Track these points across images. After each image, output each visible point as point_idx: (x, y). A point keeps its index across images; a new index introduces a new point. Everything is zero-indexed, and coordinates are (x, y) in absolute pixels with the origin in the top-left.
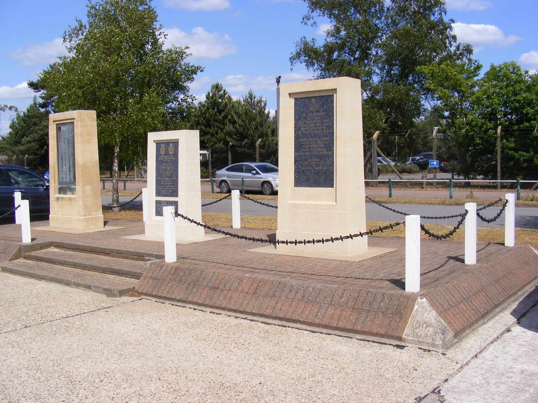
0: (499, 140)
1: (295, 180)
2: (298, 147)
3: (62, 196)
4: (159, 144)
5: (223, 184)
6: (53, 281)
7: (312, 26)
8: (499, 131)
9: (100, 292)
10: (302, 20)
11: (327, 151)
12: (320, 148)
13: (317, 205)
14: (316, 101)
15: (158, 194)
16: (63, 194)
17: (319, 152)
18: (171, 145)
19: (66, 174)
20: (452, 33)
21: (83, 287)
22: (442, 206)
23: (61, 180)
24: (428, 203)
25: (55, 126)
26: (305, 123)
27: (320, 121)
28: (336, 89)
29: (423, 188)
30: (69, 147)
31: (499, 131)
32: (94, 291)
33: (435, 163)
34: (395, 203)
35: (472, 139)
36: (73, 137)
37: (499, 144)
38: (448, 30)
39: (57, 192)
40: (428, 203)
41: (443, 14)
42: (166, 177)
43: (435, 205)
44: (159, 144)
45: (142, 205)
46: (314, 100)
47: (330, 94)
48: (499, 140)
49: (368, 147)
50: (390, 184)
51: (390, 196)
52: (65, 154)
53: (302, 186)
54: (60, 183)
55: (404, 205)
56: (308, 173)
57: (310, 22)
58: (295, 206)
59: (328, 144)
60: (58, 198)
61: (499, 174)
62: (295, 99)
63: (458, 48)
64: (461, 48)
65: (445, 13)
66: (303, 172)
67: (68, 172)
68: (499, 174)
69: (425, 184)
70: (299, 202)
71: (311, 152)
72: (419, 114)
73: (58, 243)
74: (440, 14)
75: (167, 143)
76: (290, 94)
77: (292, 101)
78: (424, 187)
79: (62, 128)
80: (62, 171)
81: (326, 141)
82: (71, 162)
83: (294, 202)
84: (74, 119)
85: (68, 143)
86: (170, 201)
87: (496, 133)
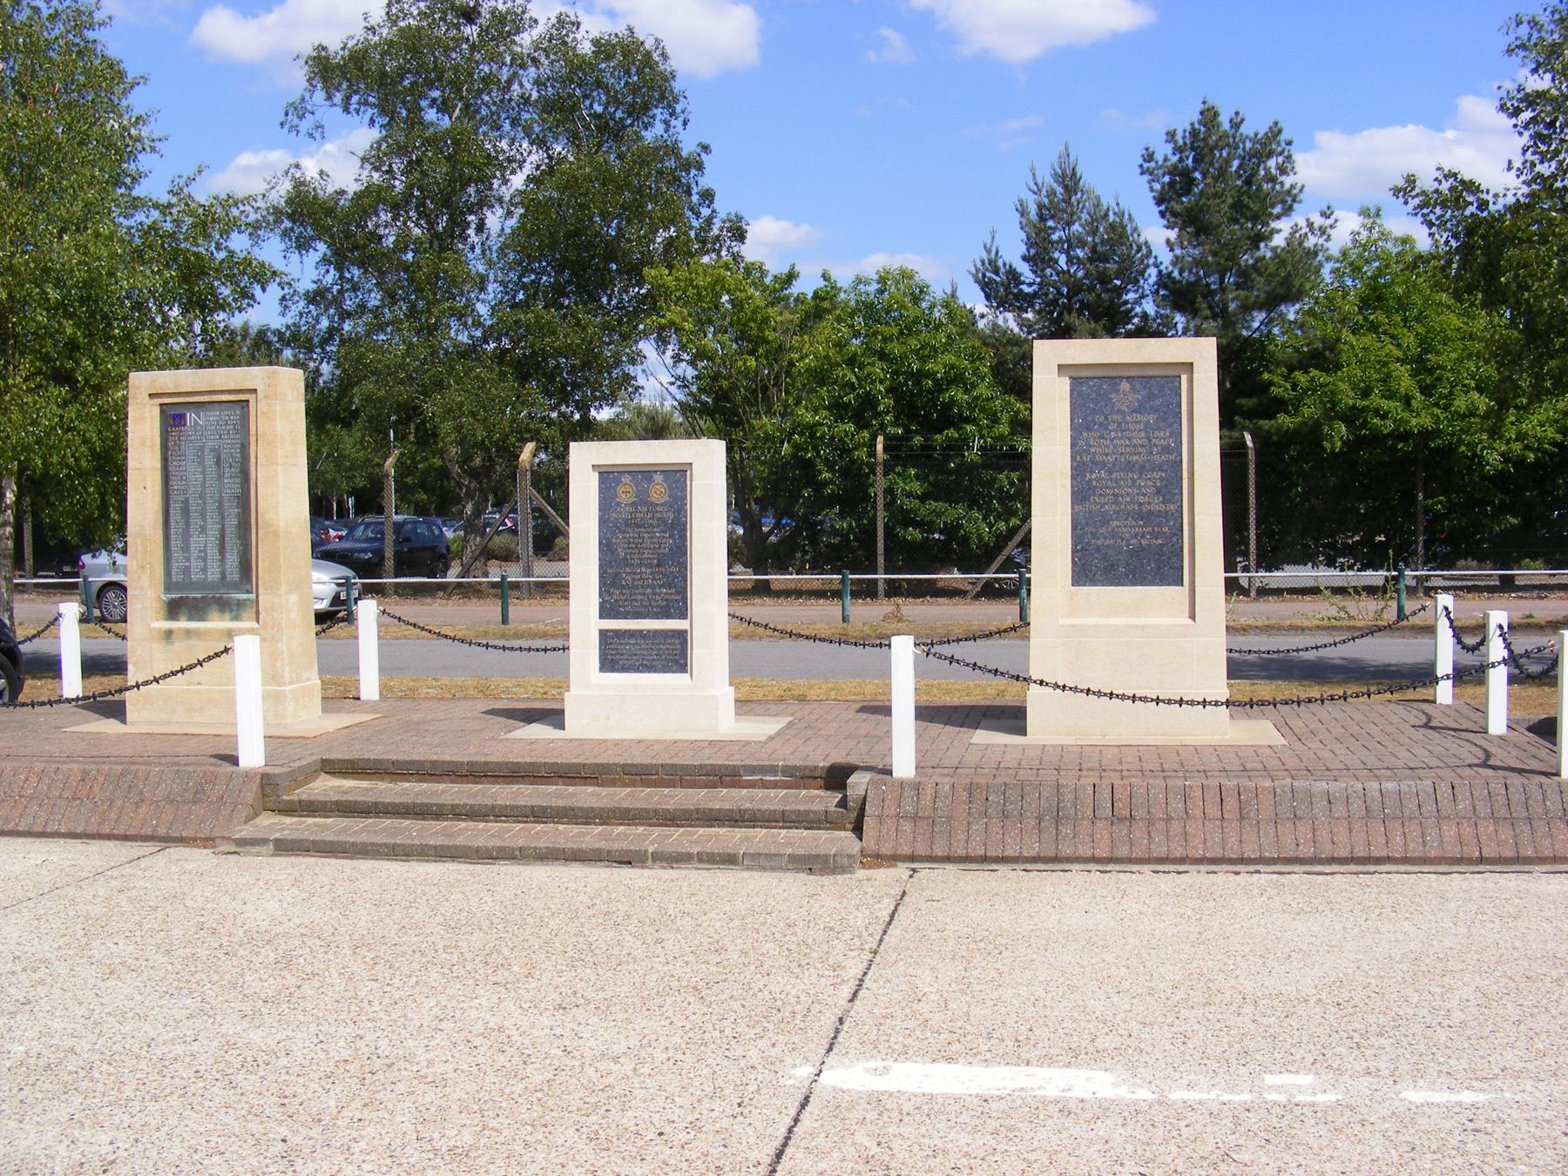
0: (879, 470)
2: (1081, 493)
3: (182, 624)
4: (678, 476)
5: (111, 595)
6: (557, 859)
7: (311, 135)
8: (880, 447)
9: (781, 869)
10: (282, 118)
13: (1143, 627)
14: (1133, 388)
15: (606, 611)
16: (190, 619)
18: (658, 478)
19: (204, 559)
21: (700, 861)
23: (177, 577)
25: (157, 411)
26: (1102, 437)
27: (1143, 434)
30: (220, 477)
31: (880, 447)
32: (748, 868)
35: (808, 466)
36: (244, 448)
37: (880, 483)
39: (162, 613)
42: (641, 565)
44: (609, 477)
45: (59, 662)
46: (1125, 386)
47: (1171, 372)
48: (879, 470)
49: (468, 487)
50: (503, 590)
51: (505, 620)
52: (202, 496)
53: (1093, 582)
54: (169, 586)
56: (1110, 552)
57: (306, 124)
60: (169, 634)
61: (881, 560)
67: (213, 553)
68: (881, 560)
69: (881, 587)
70: (1092, 621)
71: (1116, 502)
72: (610, 399)
73: (351, 762)
75: (644, 474)
76: (1060, 366)
77: (1065, 384)
79: (191, 417)
80: (186, 548)
81: (1161, 479)
82: (232, 522)
83: (1078, 621)
84: (255, 391)
85: (218, 463)
86: (673, 631)
87: (872, 454)
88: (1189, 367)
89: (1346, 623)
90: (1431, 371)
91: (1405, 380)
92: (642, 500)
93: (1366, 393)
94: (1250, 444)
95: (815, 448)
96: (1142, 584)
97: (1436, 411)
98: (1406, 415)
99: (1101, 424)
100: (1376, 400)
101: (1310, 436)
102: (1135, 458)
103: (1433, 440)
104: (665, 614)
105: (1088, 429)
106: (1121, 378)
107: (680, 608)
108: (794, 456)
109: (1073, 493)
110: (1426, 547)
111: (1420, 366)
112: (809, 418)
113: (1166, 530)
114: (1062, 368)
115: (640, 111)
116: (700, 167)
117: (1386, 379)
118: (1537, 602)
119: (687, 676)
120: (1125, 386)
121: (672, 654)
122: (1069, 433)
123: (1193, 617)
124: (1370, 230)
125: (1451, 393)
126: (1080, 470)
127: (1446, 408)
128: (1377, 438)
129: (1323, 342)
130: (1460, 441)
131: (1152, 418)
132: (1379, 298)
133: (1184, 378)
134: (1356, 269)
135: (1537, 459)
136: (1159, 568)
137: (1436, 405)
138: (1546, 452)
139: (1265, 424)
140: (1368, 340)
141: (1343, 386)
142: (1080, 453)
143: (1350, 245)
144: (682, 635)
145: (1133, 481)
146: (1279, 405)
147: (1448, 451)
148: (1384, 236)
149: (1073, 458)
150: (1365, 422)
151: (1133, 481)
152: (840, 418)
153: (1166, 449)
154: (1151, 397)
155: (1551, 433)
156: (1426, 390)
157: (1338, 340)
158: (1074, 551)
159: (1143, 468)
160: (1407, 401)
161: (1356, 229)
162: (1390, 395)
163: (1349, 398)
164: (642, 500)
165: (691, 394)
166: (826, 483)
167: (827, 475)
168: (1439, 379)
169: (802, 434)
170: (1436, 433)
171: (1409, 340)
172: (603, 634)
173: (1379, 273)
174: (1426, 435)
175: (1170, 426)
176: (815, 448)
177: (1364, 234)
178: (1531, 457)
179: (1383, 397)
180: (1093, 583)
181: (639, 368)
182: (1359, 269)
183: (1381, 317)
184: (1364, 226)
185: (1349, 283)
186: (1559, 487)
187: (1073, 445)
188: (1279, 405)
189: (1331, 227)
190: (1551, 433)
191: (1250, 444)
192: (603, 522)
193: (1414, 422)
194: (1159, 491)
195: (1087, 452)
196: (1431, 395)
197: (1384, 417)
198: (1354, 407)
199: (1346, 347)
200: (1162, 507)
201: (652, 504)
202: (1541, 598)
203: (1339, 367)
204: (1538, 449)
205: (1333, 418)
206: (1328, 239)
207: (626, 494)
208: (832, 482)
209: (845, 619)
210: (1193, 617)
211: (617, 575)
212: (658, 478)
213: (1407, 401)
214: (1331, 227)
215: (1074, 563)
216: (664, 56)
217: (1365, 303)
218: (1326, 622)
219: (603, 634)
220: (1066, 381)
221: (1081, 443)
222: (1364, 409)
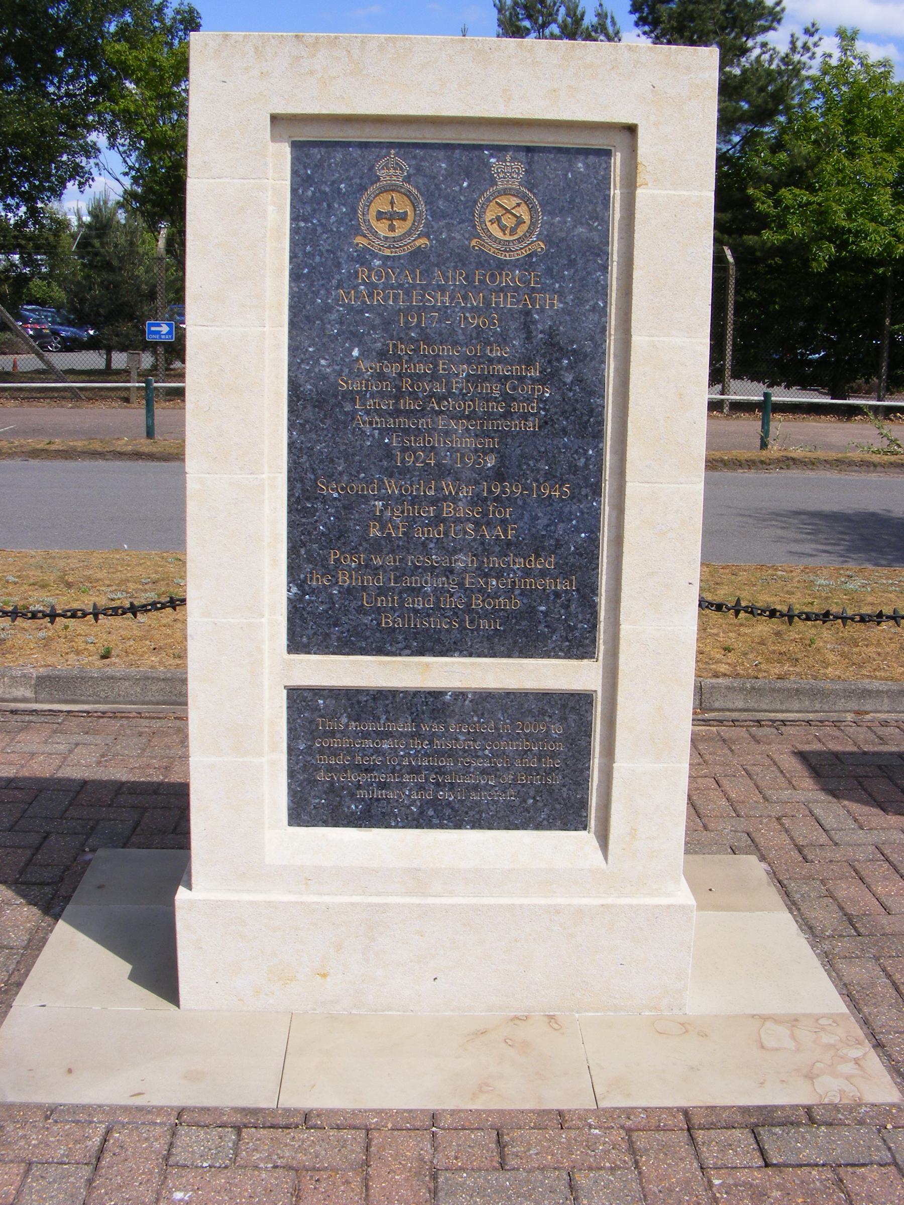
4: (577, 168)
15: (309, 628)
18: (508, 172)
29: (127, 400)
33: (165, 329)
75: (450, 159)
92: (449, 253)
94: (731, 259)
101: (795, 253)
104: (522, 635)
107: (569, 616)
110: (890, 368)
119: (586, 839)
121: (542, 773)
139: (750, 239)
146: (763, 222)
164: (449, 253)
172: (301, 700)
181: (92, 161)
188: (763, 222)
191: (731, 259)
192: (302, 316)
201: (485, 261)
205: (821, 239)
207: (389, 221)
211: (349, 505)
212: (508, 172)
219: (301, 700)
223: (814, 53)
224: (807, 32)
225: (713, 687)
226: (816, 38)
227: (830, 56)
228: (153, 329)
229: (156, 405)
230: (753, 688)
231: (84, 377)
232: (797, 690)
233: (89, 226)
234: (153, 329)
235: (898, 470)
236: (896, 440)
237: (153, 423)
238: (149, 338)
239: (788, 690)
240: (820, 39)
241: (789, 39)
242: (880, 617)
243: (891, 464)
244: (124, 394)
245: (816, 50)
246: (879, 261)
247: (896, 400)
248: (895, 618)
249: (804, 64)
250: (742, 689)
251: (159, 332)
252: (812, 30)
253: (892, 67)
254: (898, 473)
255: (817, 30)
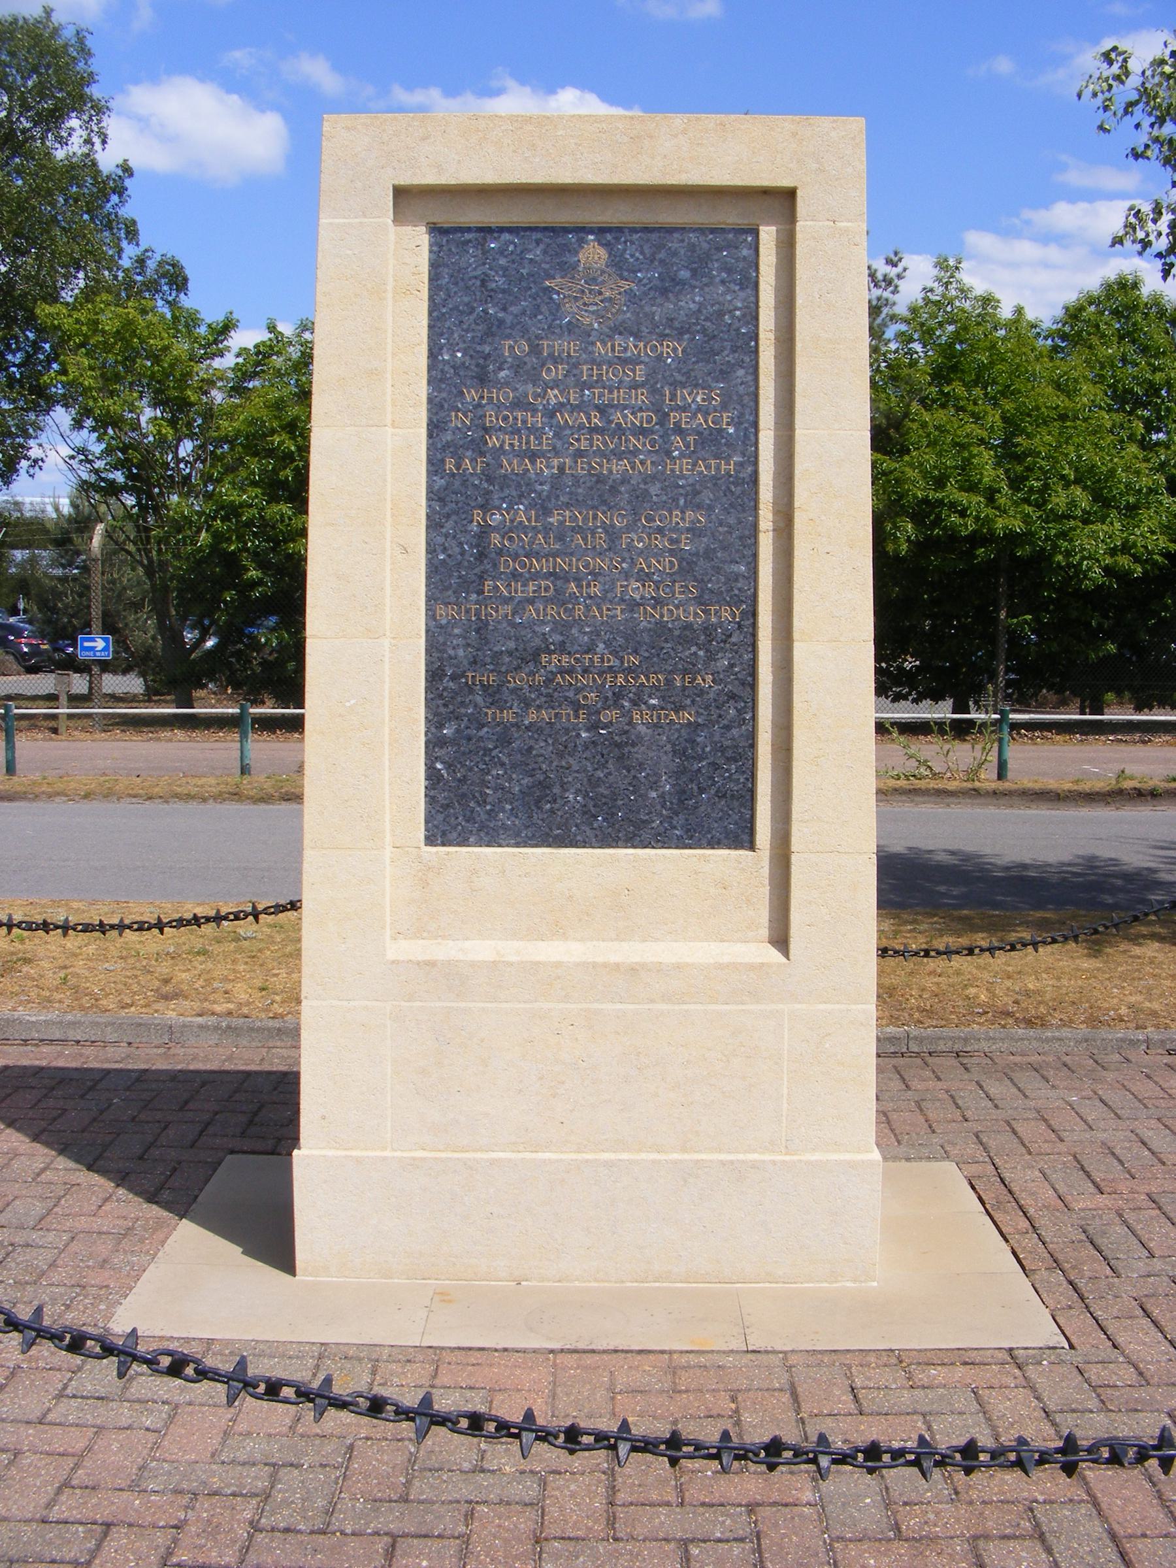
1: (431, 799)
2: (460, 563)
11: (700, 601)
12: (644, 577)
13: (634, 970)
14: (617, 264)
17: (633, 605)
20: (126, 212)
22: (232, 807)
24: (177, 796)
26: (519, 404)
27: (641, 397)
28: (790, 195)
29: (55, 731)
33: (100, 644)
34: (50, 796)
35: (232, 563)
38: (115, 199)
40: (177, 796)
41: (97, 140)
43: (204, 800)
46: (593, 254)
47: (729, 216)
55: (86, 806)
56: (542, 747)
58: (451, 978)
59: (708, 554)
62: (436, 230)
63: (141, 262)
64: (151, 265)
65: (104, 142)
66: (504, 740)
70: (481, 950)
71: (560, 599)
74: (88, 141)
76: (401, 194)
77: (412, 249)
78: (62, 729)
81: (695, 532)
83: (444, 950)
88: (783, 201)
89: (933, 784)
90: (1018, 458)
91: (988, 470)
93: (940, 483)
95: (241, 538)
96: (632, 841)
97: (1028, 509)
98: (990, 511)
99: (518, 367)
100: (952, 492)
102: (618, 467)
103: (1022, 546)
105: (482, 379)
106: (582, 230)
108: (214, 548)
109: (434, 570)
111: (1008, 454)
112: (234, 497)
113: (705, 681)
114: (407, 199)
115: (53, 119)
116: (121, 191)
117: (965, 466)
118: (1140, 746)
120: (593, 254)
122: (421, 389)
123: (781, 941)
124: (947, 284)
125: (1046, 486)
126: (453, 501)
127: (1039, 506)
128: (953, 537)
129: (887, 417)
130: (1055, 547)
131: (671, 350)
132: (954, 368)
133: (768, 235)
134: (927, 335)
135: (1145, 572)
136: (682, 795)
137: (1026, 501)
138: (1155, 564)
140: (941, 416)
141: (912, 474)
142: (453, 448)
143: (920, 302)
144: (303, 715)
145: (613, 535)
147: (1041, 559)
148: (964, 292)
149: (435, 466)
150: (938, 518)
151: (613, 535)
152: (273, 499)
153: (710, 441)
154: (668, 287)
155: (1163, 542)
156: (1016, 483)
157: (906, 415)
158: (434, 743)
159: (640, 498)
160: (991, 495)
161: (930, 284)
162: (971, 487)
163: (919, 490)
165: (97, 472)
166: (254, 584)
167: (253, 574)
168: (1029, 469)
169: (225, 519)
170: (1027, 537)
171: (994, 417)
173: (957, 337)
174: (1012, 538)
175: (724, 374)
176: (241, 538)
177: (940, 290)
178: (1139, 570)
179: (961, 489)
180: (491, 836)
182: (930, 332)
183: (958, 388)
184: (939, 280)
185: (917, 347)
186: (1166, 608)
187: (435, 428)
189: (899, 277)
190: (1163, 542)
193: (1000, 523)
194: (687, 567)
195: (479, 447)
196: (1018, 490)
197: (963, 514)
198: (925, 501)
199: (915, 426)
200: (694, 615)
202: (1144, 742)
203: (905, 451)
204: (1146, 561)
205: (897, 515)
206: (895, 291)
208: (260, 583)
209: (245, 770)
210: (781, 941)
213: (991, 495)
214: (899, 277)
215: (432, 776)
216: (86, 52)
217: (940, 375)
218: (902, 783)
220: (418, 240)
221: (456, 420)
222: (941, 502)
223: (896, 287)
224: (889, 262)
225: (184, 1026)
226: (899, 269)
227: (931, 290)
228: (86, 644)
229: (17, 738)
230: (229, 1027)
231: (27, 703)
232: (279, 1030)
233: (70, 520)
234: (86, 644)
235: (904, 798)
236: (926, 761)
237: (14, 758)
238: (82, 656)
239: (269, 1030)
240: (905, 270)
241: (867, 272)
242: (46, 926)
243: (896, 790)
244: (53, 724)
245: (900, 283)
246: (976, 539)
247: (1062, 713)
248: (10, 926)
249: (887, 300)
250: (217, 1028)
251: (92, 649)
252: (895, 259)
253: (998, 301)
254: (903, 802)
255: (900, 260)
